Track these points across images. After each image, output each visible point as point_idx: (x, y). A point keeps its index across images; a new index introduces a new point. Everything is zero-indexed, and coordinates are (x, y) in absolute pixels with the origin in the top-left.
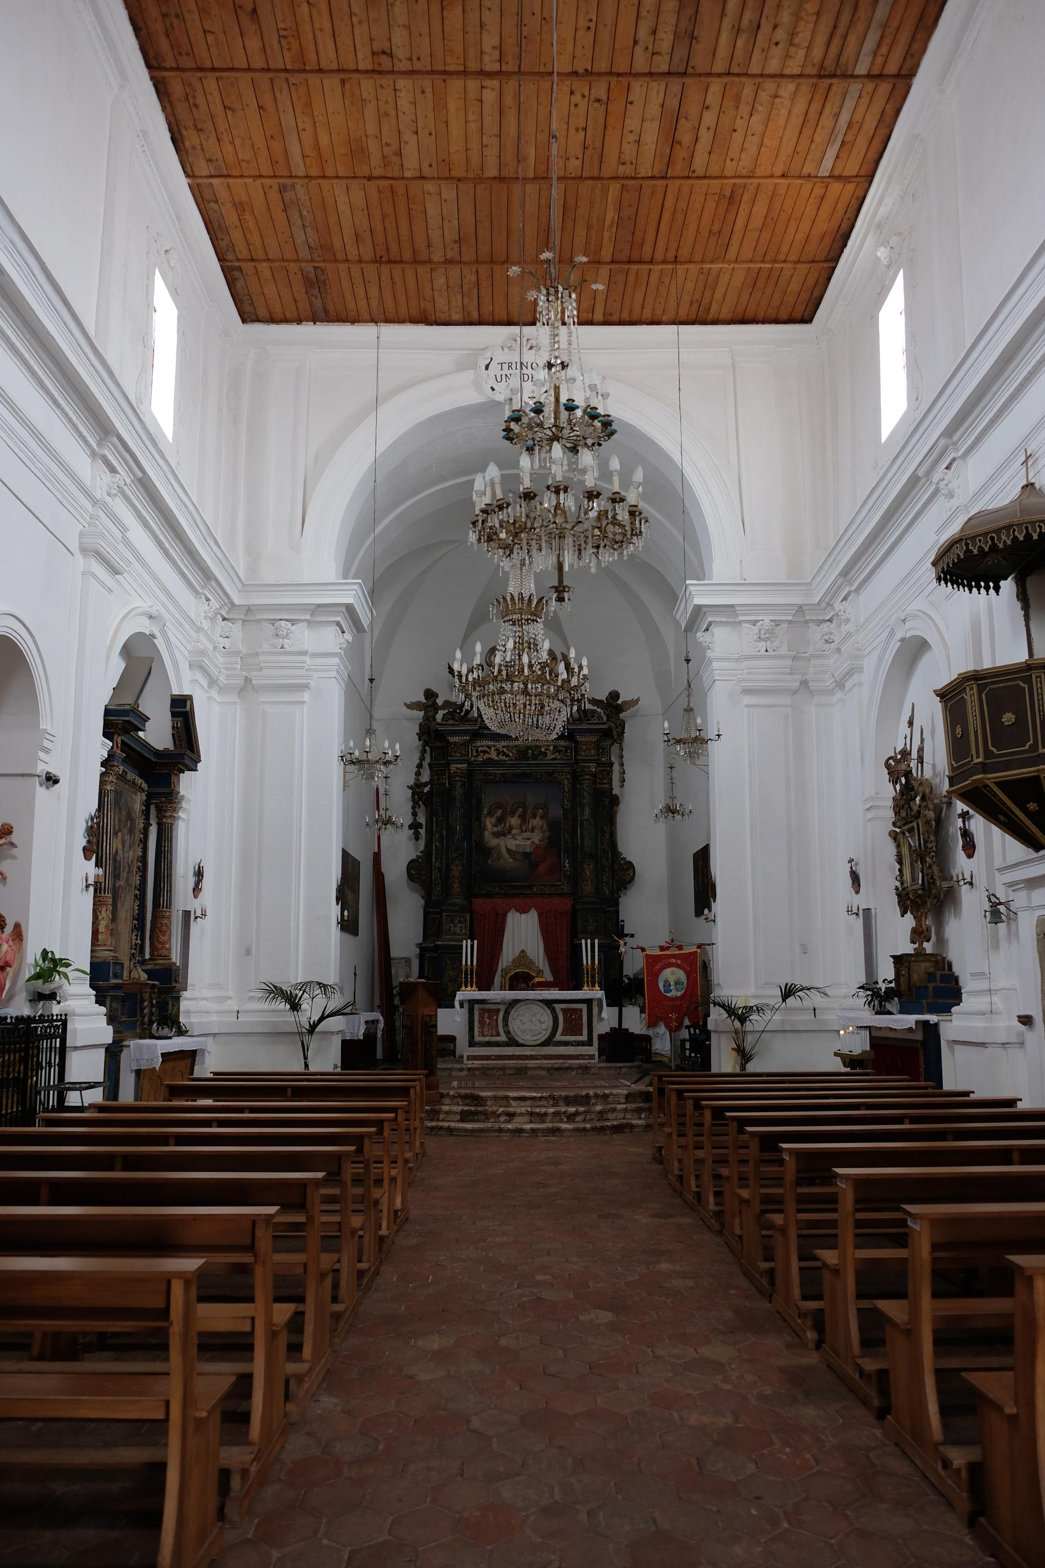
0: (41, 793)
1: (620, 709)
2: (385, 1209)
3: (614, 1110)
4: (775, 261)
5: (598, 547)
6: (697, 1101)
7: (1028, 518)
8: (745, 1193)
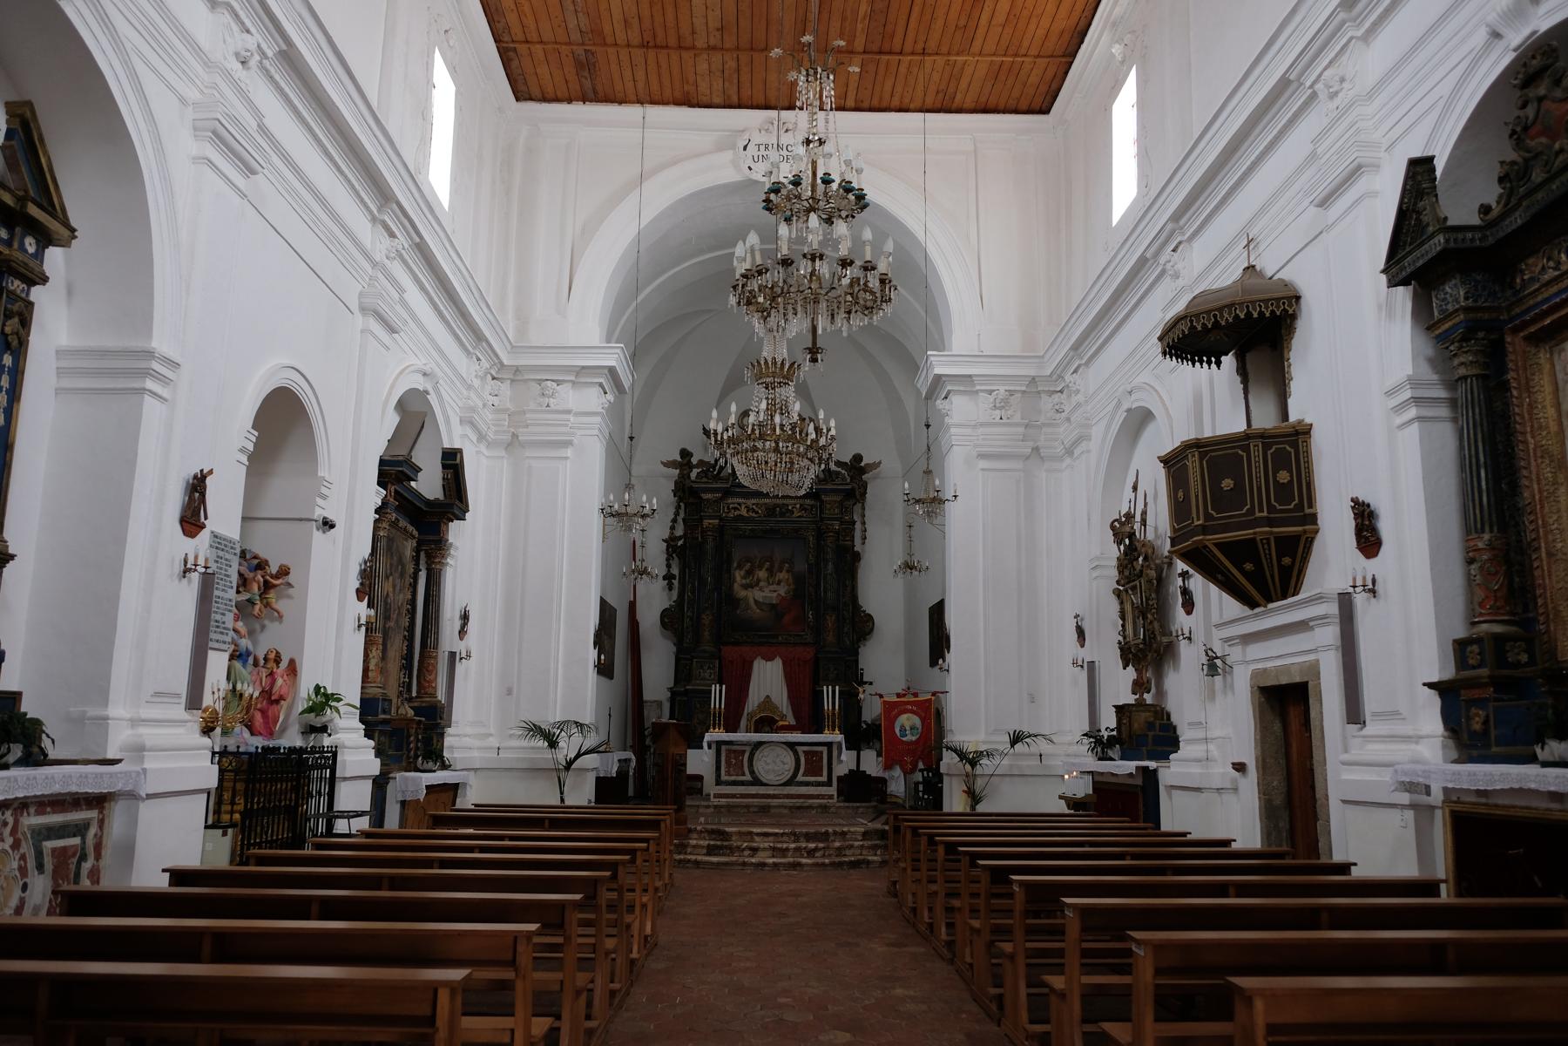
0: (318, 536)
1: (863, 471)
2: (636, 934)
3: (852, 847)
4: (1016, 55)
5: (849, 312)
6: (931, 837)
7: (1248, 298)
8: (976, 924)
